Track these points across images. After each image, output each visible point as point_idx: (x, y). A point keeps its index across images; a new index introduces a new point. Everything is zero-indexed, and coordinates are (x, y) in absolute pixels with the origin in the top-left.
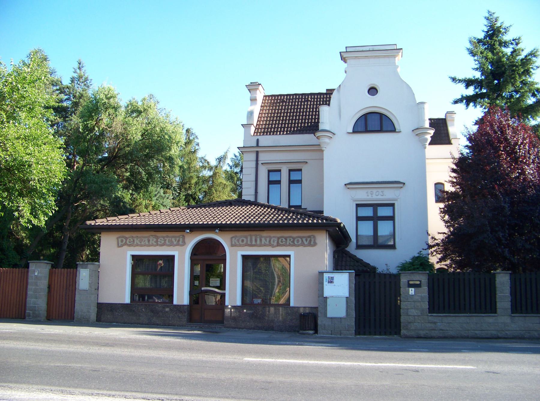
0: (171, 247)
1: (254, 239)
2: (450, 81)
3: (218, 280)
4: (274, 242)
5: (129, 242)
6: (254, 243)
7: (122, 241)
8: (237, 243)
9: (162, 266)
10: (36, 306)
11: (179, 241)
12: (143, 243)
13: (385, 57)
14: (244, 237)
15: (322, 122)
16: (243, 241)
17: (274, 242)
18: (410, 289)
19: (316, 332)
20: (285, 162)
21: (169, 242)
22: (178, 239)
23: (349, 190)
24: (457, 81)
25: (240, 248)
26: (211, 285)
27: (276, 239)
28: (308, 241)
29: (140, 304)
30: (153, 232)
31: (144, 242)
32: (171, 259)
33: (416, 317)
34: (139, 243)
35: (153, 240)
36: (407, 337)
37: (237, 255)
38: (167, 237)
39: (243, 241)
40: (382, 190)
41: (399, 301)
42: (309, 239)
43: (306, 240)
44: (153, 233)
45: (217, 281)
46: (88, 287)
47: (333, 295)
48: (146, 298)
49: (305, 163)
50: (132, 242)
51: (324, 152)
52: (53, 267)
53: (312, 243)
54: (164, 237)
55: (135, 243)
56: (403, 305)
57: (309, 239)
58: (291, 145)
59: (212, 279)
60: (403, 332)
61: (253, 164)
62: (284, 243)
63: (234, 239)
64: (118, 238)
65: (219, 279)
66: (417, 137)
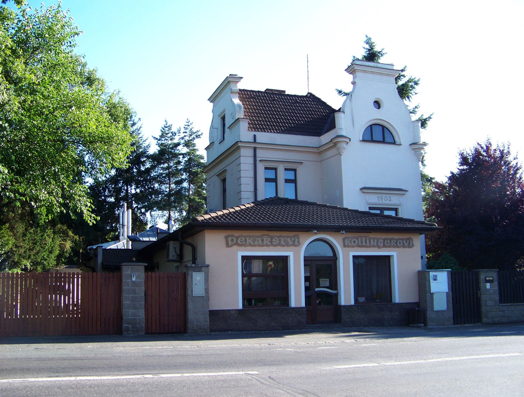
3: (327, 281)
4: (381, 243)
5: (241, 241)
6: (364, 244)
7: (232, 240)
8: (350, 244)
10: (136, 319)
12: (256, 243)
13: (387, 75)
14: (355, 238)
15: (341, 128)
16: (354, 242)
17: (381, 243)
18: (487, 284)
19: (425, 325)
22: (293, 239)
23: (363, 194)
26: (321, 286)
27: (382, 241)
29: (257, 309)
30: (265, 231)
32: (285, 259)
33: (492, 307)
34: (252, 243)
35: (267, 240)
36: (487, 325)
39: (354, 242)
42: (408, 241)
43: (406, 242)
44: (266, 233)
47: (437, 291)
49: (301, 163)
52: (147, 269)
55: (248, 243)
57: (408, 241)
59: (323, 280)
60: (484, 320)
61: (251, 160)
62: (389, 244)
63: (346, 240)
65: (328, 280)
66: (413, 151)
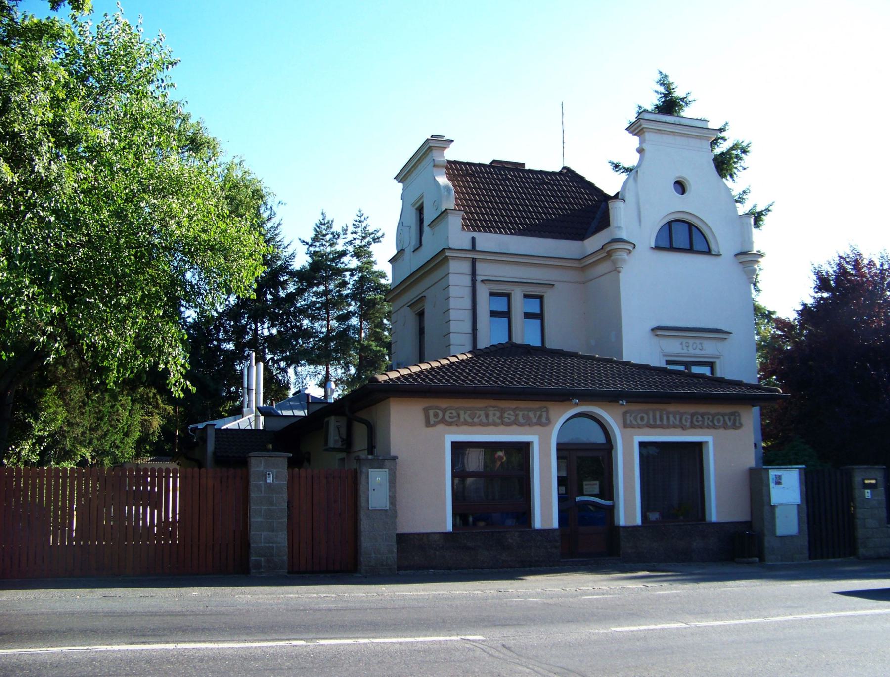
0: (527, 428)
1: (658, 417)
2: (611, 167)
4: (686, 421)
5: (450, 417)
6: (658, 422)
7: (436, 415)
8: (634, 423)
9: (504, 461)
10: (273, 547)
11: (540, 417)
12: (476, 420)
13: (696, 137)
16: (642, 419)
17: (686, 421)
18: (866, 491)
20: (517, 282)
21: (523, 419)
22: (538, 413)
24: (620, 169)
25: (637, 430)
26: (585, 493)
27: (689, 417)
28: (732, 421)
30: (492, 400)
31: (478, 418)
32: (524, 448)
34: (469, 420)
35: (494, 415)
37: (632, 441)
38: (521, 410)
39: (642, 419)
40: (701, 341)
41: (852, 509)
43: (730, 420)
45: (595, 486)
46: (388, 506)
48: (471, 519)
50: (456, 417)
51: (620, 274)
52: (293, 464)
53: (736, 425)
54: (514, 410)
56: (860, 513)
58: (528, 254)
60: (862, 551)
61: (468, 280)
62: (700, 423)
64: (426, 411)
